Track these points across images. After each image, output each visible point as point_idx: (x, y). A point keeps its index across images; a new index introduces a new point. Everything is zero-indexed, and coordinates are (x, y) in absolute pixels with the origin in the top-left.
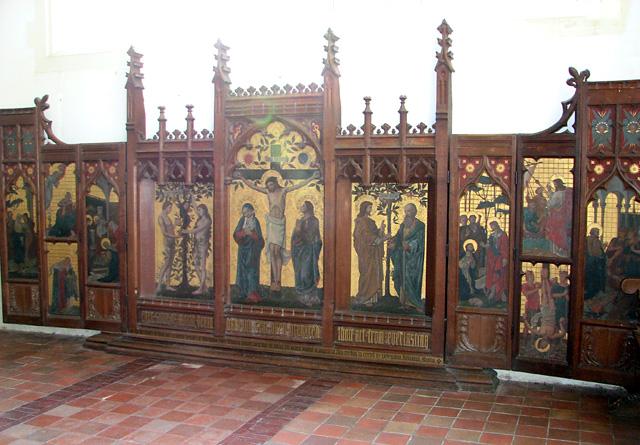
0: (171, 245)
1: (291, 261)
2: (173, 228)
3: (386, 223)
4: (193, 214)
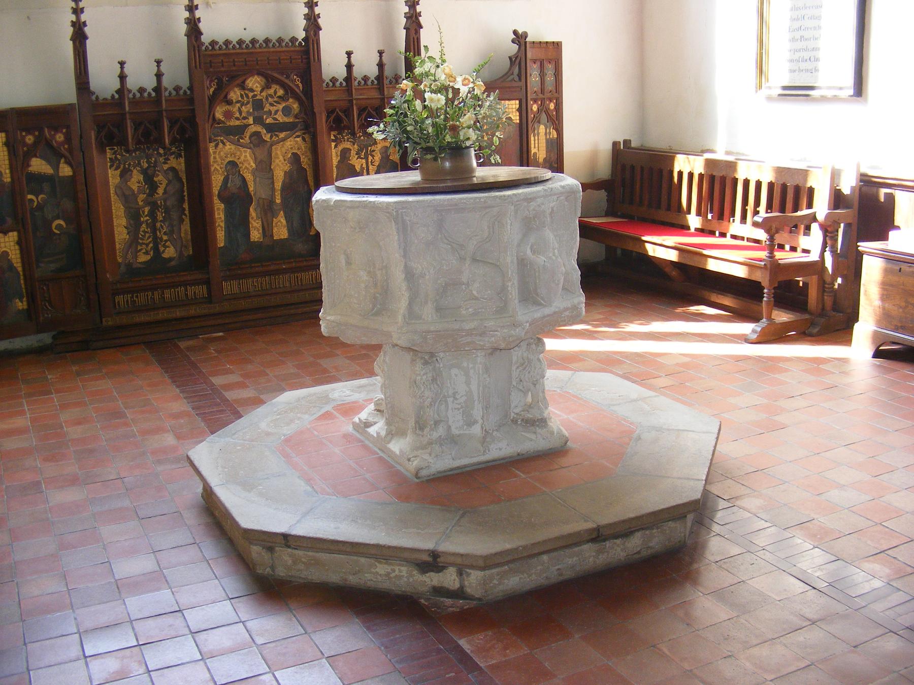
0: (134, 216)
1: (282, 212)
2: (136, 197)
3: (364, 166)
4: (160, 178)
